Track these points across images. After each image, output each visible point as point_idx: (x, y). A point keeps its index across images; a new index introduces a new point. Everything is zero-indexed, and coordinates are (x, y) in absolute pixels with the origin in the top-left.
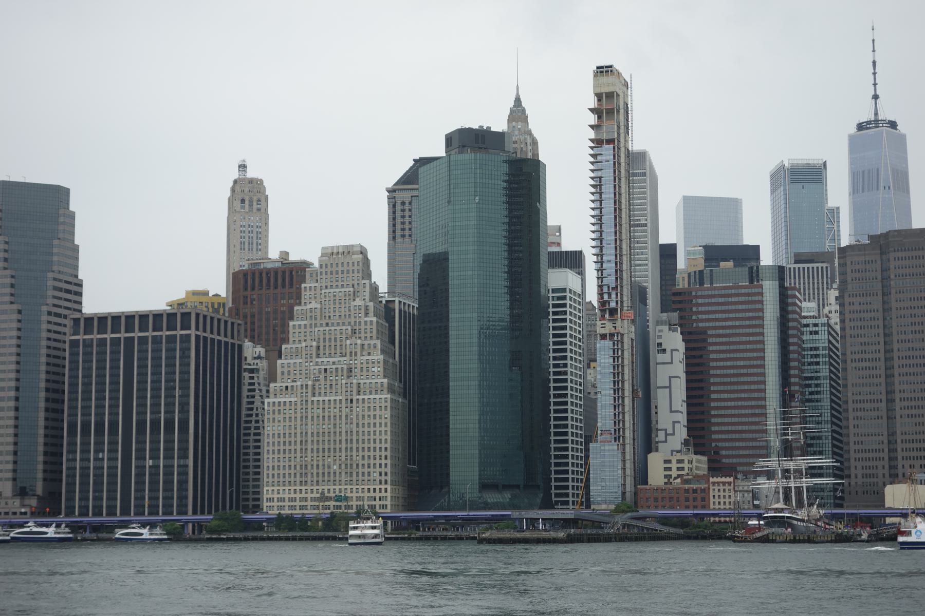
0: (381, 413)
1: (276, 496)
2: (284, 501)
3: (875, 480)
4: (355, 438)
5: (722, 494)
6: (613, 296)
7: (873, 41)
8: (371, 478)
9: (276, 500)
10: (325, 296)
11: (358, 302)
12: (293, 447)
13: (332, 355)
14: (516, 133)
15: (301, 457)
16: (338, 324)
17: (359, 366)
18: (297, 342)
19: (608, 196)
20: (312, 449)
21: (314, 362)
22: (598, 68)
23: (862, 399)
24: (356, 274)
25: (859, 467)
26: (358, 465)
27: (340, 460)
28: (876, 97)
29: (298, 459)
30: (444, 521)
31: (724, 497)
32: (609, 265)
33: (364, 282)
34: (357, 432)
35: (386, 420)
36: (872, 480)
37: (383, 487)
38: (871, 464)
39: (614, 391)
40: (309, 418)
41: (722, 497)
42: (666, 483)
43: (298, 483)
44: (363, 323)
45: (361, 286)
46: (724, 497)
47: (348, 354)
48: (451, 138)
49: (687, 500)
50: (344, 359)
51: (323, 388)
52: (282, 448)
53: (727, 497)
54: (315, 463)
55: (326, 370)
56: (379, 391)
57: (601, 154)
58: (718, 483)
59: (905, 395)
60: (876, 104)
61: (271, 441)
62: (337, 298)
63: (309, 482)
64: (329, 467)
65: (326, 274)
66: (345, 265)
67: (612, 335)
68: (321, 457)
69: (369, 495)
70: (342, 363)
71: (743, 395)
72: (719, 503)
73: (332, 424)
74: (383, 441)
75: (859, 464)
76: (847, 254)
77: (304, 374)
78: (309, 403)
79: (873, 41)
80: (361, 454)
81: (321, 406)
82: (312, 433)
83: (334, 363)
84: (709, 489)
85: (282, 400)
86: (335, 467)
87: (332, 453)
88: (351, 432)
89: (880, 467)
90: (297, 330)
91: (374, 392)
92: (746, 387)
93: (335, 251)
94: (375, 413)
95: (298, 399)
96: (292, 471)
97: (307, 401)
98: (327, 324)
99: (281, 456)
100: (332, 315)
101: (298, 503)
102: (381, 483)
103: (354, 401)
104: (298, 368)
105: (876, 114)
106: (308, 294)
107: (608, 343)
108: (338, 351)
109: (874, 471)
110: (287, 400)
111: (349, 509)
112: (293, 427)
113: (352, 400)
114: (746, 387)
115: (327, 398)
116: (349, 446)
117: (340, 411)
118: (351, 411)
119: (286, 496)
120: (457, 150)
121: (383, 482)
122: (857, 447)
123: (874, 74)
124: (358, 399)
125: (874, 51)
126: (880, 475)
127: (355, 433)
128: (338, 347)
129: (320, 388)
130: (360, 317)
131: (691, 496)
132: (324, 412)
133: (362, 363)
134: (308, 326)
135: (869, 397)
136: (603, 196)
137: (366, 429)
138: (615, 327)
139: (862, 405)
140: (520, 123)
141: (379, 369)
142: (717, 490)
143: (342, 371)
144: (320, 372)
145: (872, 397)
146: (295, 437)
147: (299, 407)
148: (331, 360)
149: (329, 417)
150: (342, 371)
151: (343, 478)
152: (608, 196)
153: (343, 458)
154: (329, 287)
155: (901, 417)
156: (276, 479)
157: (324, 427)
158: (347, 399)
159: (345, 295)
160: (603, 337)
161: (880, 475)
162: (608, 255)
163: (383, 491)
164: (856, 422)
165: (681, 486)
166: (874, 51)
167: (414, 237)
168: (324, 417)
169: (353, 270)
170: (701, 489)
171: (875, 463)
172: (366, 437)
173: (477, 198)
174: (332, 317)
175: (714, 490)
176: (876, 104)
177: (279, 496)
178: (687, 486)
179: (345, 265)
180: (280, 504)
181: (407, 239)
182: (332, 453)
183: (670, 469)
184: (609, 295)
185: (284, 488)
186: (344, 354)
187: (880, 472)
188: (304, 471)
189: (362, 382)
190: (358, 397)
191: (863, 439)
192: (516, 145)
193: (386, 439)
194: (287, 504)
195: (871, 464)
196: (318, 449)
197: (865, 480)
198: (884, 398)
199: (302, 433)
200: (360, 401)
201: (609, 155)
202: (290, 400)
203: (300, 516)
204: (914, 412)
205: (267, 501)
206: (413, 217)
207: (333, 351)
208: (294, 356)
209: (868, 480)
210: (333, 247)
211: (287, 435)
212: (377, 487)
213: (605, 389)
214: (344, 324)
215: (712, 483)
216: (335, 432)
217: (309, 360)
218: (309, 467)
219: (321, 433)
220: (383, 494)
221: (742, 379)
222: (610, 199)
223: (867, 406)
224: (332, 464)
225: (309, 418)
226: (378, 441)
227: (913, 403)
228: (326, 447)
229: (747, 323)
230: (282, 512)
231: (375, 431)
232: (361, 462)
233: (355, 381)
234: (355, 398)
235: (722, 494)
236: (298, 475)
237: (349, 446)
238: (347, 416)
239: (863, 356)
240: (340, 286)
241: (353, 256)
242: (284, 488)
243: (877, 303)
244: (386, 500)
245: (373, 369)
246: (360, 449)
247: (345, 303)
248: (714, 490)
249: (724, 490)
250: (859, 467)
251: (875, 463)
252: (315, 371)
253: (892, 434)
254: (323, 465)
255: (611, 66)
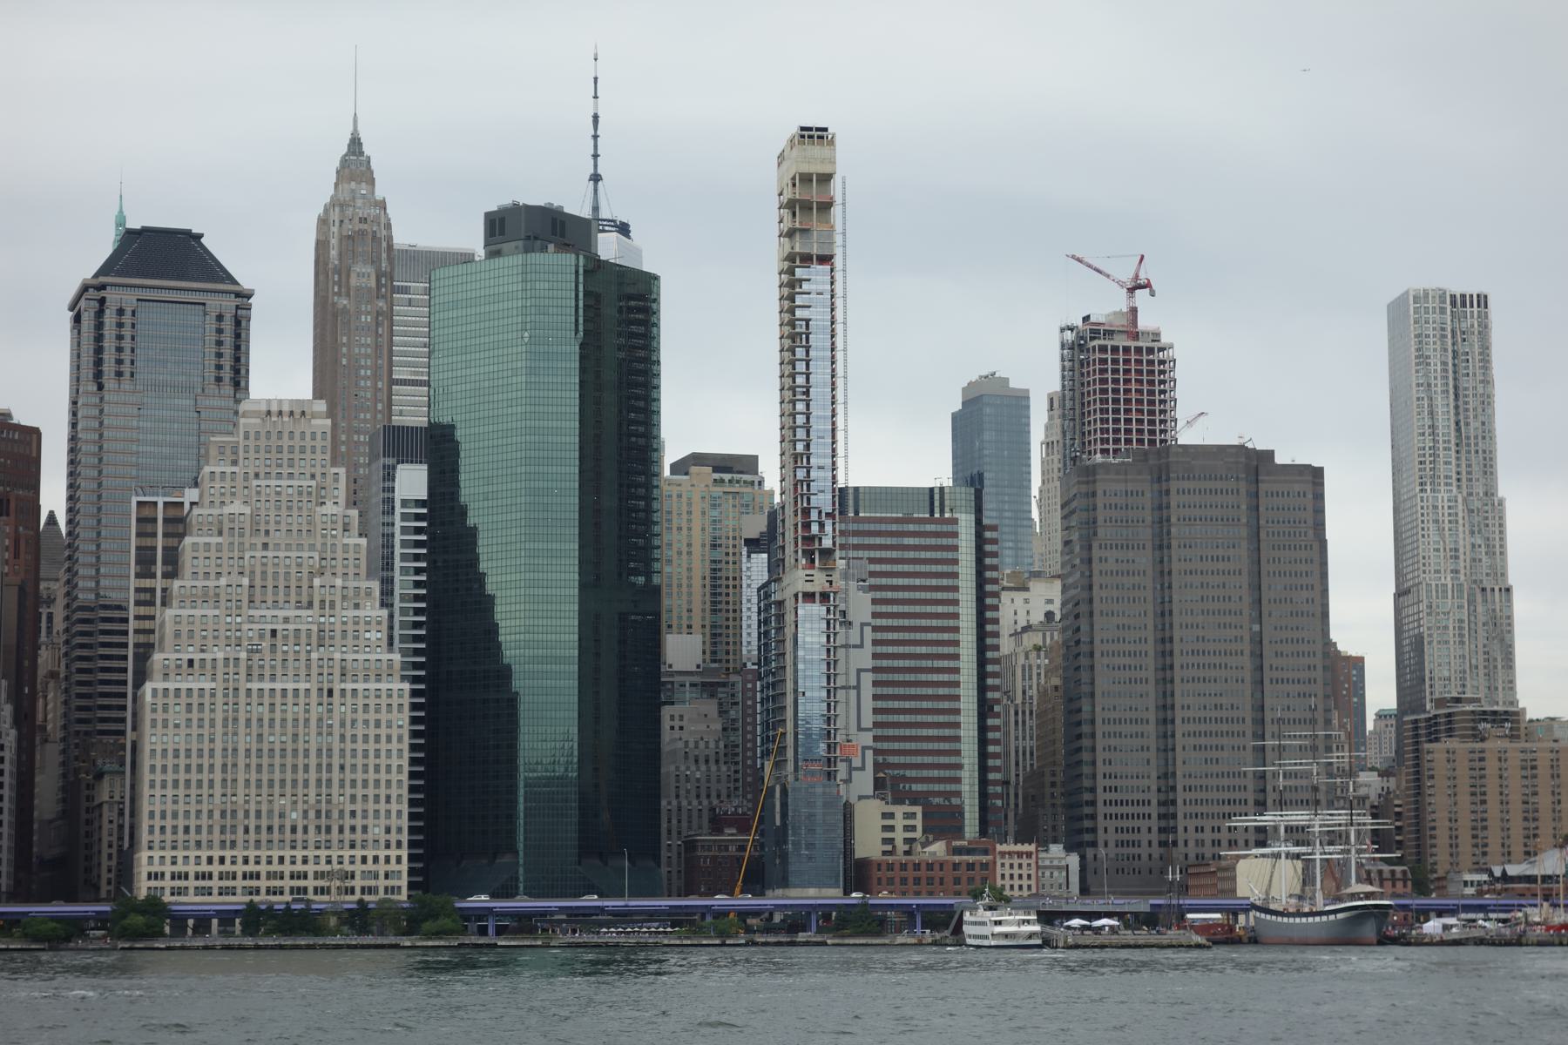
0: (390, 716)
1: (168, 869)
2: (234, 878)
3: (1136, 851)
4: (336, 762)
5: (1016, 872)
6: (828, 528)
7: (596, 79)
8: (370, 837)
9: (168, 876)
10: (258, 493)
11: (329, 508)
12: (205, 777)
13: (281, 604)
14: (359, 203)
15: (224, 795)
16: (288, 547)
17: (338, 628)
18: (201, 576)
19: (821, 354)
20: (247, 781)
21: (245, 617)
22: (803, 129)
23: (1117, 717)
24: (319, 456)
25: (1111, 830)
26: (341, 812)
27: (305, 802)
28: (596, 178)
29: (217, 799)
30: (564, 917)
31: (1020, 876)
32: (821, 474)
33: (335, 470)
34: (342, 750)
35: (401, 731)
36: (1131, 850)
37: (393, 853)
38: (1129, 824)
39: (829, 691)
40: (242, 721)
41: (1016, 877)
42: (884, 853)
43: (216, 843)
44: (339, 549)
45: (329, 479)
46: (1020, 876)
47: (316, 604)
48: (502, 220)
49: (957, 881)
50: (309, 612)
51: (267, 667)
52: (182, 777)
53: (1025, 877)
54: (253, 808)
55: (274, 632)
56: (384, 676)
57: (809, 280)
58: (1010, 853)
59: (1190, 714)
60: (596, 190)
61: (159, 764)
62: (284, 498)
63: (240, 843)
64: (282, 815)
65: (257, 452)
66: (297, 435)
67: (825, 597)
68: (265, 795)
69: (364, 867)
70: (304, 620)
71: (925, 705)
72: (1021, 887)
73: (290, 736)
74: (394, 769)
75: (1112, 824)
76: (1098, 477)
77: (222, 637)
78: (242, 693)
79: (596, 79)
80: (348, 791)
81: (267, 701)
82: (248, 750)
83: (286, 620)
84: (995, 863)
85: (184, 686)
86: (294, 815)
87: (288, 789)
88: (330, 750)
89: (1144, 830)
90: (201, 554)
91: (373, 677)
92: (930, 691)
93: (274, 408)
94: (378, 716)
95: (218, 685)
96: (204, 822)
97: (236, 689)
98: (265, 546)
99: (181, 791)
100: (272, 527)
101: (263, 884)
102: (388, 846)
103: (336, 694)
104: (211, 627)
105: (596, 209)
106: (218, 486)
107: (818, 609)
108: (293, 598)
109: (1135, 837)
110: (195, 686)
111: (393, 893)
112: (206, 738)
113: (330, 692)
114: (930, 691)
115: (278, 686)
116: (325, 776)
117: (307, 711)
118: (330, 711)
119: (192, 869)
120: (520, 243)
121: (394, 844)
122: (1109, 796)
123: (595, 137)
124: (343, 690)
125: (596, 97)
126: (1145, 843)
127: (336, 752)
128: (293, 590)
129: (262, 667)
130: (334, 537)
131: (963, 873)
132: (272, 711)
133: (344, 623)
134: (225, 547)
135: (1128, 715)
136: (812, 353)
137: (360, 746)
138: (831, 582)
139: (1118, 728)
140: (364, 185)
141: (379, 635)
142: (1007, 866)
143: (309, 636)
144: (261, 637)
145: (1134, 715)
146: (212, 756)
147: (220, 699)
148: (281, 614)
149: (284, 720)
150: (309, 636)
151: (312, 836)
152: (821, 354)
153: (312, 798)
154: (262, 475)
155: (1184, 748)
156: (169, 836)
157: (284, 739)
158: (320, 690)
159: (300, 493)
160: (809, 597)
161: (1145, 843)
162: (819, 456)
163: (393, 860)
164: (1107, 755)
165: (948, 858)
166: (596, 97)
167: (137, 376)
168: (272, 720)
169: (313, 447)
170: (982, 864)
171: (1136, 823)
172: (360, 761)
173: (526, 334)
174: (272, 533)
175: (1003, 865)
176: (596, 190)
177: (176, 869)
178: (957, 859)
179: (297, 435)
180: (177, 883)
181: (126, 384)
182: (288, 789)
183: (891, 828)
184: (822, 525)
185: (186, 853)
186: (305, 603)
187: (1144, 837)
188: (323, 821)
189: (350, 657)
190: (343, 686)
191: (1118, 783)
192: (365, 226)
193: (400, 766)
194: (192, 883)
195: (1129, 824)
196: (259, 781)
197: (1120, 850)
198: (1152, 716)
199: (225, 750)
200: (349, 694)
201: (823, 283)
202: (178, 685)
203: (282, 907)
204: (1203, 741)
205: (399, 888)
206: (138, 339)
207: (281, 598)
208: (199, 602)
209: (1125, 851)
210: (269, 401)
211: (194, 754)
212: (382, 854)
213: (812, 689)
214: (300, 547)
215: (1000, 853)
216: (295, 751)
217: (234, 612)
218: (241, 814)
219: (266, 751)
220: (393, 866)
221: (923, 677)
222: (823, 359)
223: (1126, 729)
224: (288, 807)
225: (242, 721)
226: (383, 769)
227: (1203, 727)
228: (277, 776)
229: (934, 582)
230: (256, 899)
231: (377, 750)
232: (348, 808)
233: (337, 656)
234: (337, 687)
235: (1016, 872)
236: (217, 830)
237: (325, 776)
238: (320, 720)
239: (1121, 647)
240: (285, 475)
241: (314, 422)
242: (186, 853)
243: (1145, 560)
244: (400, 878)
245: (368, 635)
246: (348, 783)
247: (300, 509)
248: (1003, 865)
249: (1020, 866)
250: (1111, 830)
251: (1136, 823)
252: (251, 634)
253: (1167, 775)
254: (270, 812)
255: (825, 130)
